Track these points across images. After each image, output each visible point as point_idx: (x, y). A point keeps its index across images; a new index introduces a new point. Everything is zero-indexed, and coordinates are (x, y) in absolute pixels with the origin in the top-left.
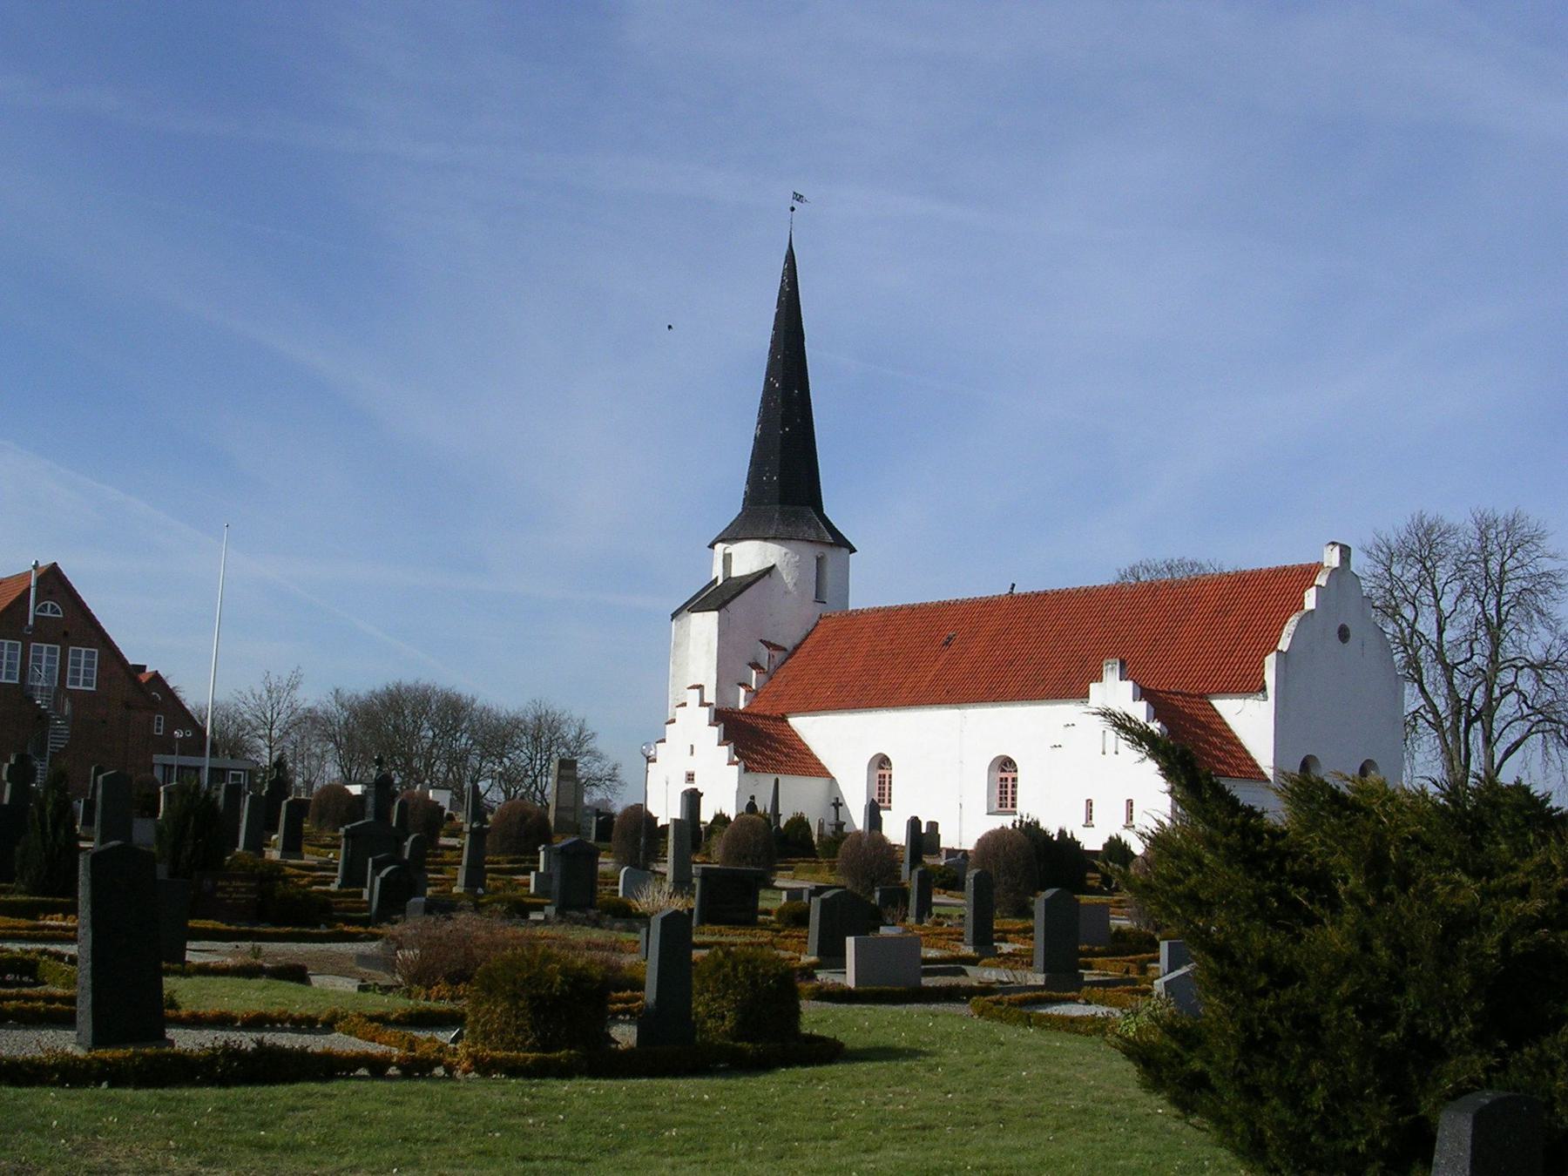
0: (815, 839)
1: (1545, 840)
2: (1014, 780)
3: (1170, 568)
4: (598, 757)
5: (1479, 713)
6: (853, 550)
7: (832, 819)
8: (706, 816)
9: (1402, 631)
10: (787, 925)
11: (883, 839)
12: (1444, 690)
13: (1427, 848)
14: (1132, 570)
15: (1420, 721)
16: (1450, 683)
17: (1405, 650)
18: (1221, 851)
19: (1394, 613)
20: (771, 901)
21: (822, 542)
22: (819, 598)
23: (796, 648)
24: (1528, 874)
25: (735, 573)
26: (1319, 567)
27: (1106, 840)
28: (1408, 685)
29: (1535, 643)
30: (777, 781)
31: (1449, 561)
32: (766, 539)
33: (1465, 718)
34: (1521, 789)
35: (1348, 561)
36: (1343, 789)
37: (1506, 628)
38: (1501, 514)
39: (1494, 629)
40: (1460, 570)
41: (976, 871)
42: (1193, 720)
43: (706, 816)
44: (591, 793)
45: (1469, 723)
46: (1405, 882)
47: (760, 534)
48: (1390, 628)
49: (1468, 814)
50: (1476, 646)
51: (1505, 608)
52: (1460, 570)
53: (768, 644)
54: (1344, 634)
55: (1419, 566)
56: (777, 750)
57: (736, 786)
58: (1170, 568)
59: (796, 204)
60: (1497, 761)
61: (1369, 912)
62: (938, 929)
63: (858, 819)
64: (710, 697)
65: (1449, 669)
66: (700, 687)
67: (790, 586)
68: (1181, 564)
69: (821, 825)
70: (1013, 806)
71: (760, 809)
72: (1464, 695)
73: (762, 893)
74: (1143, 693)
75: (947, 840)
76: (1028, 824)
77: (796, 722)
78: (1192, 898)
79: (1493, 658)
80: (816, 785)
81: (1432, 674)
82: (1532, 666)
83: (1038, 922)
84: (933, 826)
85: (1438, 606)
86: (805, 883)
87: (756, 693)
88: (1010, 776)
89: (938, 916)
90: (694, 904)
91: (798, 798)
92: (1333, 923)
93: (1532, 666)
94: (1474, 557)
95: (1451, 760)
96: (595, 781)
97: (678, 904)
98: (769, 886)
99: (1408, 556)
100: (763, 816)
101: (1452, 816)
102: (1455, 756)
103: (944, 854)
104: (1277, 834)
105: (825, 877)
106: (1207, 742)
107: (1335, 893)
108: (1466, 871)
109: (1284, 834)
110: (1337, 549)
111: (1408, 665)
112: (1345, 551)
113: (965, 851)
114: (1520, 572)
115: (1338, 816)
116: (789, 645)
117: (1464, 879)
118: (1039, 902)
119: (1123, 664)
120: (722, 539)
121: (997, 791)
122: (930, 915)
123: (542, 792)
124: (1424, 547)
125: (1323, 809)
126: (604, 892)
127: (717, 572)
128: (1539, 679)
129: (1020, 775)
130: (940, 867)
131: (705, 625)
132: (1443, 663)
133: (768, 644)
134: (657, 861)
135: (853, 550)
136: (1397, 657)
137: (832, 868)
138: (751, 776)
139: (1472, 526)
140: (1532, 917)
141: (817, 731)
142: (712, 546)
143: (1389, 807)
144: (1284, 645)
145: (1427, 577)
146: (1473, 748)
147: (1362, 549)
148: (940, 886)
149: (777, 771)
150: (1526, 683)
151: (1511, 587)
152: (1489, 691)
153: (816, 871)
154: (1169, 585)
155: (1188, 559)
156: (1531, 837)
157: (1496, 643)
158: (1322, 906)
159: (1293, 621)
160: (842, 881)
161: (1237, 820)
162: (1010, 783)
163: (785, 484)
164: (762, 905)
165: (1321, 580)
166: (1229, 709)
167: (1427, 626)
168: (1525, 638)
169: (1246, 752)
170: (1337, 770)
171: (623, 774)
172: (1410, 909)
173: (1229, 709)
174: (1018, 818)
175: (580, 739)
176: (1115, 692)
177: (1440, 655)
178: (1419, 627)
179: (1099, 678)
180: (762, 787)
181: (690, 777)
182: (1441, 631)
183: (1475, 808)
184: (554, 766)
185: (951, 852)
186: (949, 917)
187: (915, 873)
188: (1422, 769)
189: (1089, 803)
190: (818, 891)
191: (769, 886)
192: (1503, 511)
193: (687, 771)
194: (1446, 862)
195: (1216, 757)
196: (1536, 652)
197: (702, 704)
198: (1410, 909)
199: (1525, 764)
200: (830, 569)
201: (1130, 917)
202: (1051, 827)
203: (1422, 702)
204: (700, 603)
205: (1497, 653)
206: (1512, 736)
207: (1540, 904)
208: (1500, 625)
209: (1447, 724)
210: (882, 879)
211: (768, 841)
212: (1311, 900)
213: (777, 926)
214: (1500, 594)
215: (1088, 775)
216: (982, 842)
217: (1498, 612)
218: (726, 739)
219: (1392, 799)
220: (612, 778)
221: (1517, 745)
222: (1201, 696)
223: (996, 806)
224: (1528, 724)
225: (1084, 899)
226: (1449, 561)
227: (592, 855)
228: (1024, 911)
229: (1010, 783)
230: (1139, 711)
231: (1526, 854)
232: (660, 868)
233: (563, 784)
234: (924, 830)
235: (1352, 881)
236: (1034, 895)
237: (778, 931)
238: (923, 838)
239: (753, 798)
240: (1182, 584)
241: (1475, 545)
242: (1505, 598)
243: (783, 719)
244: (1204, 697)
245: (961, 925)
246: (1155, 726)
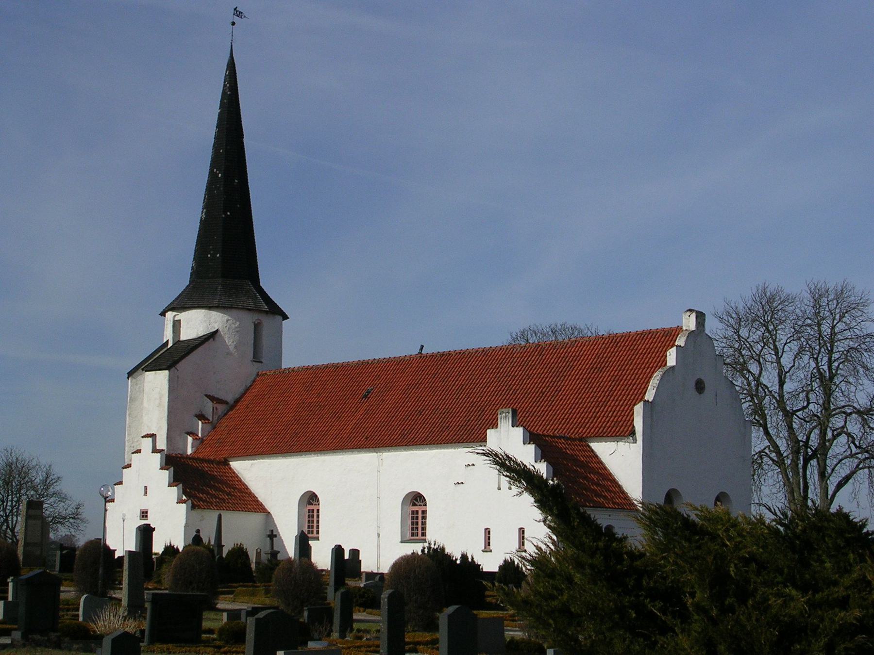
0: (253, 566)
1: (862, 559)
2: (424, 512)
3: (554, 332)
4: (62, 497)
5: (815, 453)
6: (285, 317)
7: (268, 549)
8: (158, 548)
9: (749, 384)
10: (227, 642)
11: (311, 565)
12: (785, 433)
13: (762, 566)
14: (523, 333)
15: (766, 459)
16: (790, 428)
17: (752, 400)
18: (588, 571)
19: (742, 368)
20: (214, 622)
21: (258, 310)
22: (257, 358)
23: (237, 401)
24: (847, 588)
25: (184, 337)
26: (678, 330)
27: (501, 562)
28: (754, 429)
29: (861, 392)
30: (220, 517)
31: (788, 324)
32: (210, 308)
33: (805, 456)
34: (842, 516)
35: (704, 326)
36: (693, 517)
37: (837, 380)
38: (831, 285)
39: (827, 382)
40: (798, 332)
41: (390, 591)
42: (575, 460)
43: (158, 548)
44: (56, 530)
45: (806, 461)
46: (743, 595)
48: (739, 382)
49: (798, 538)
50: (812, 396)
51: (836, 364)
52: (797, 332)
53: (212, 398)
54: (700, 386)
55: (763, 329)
56: (219, 490)
57: (184, 522)
58: (554, 332)
60: (830, 493)
61: (714, 622)
62: (358, 643)
63: (290, 548)
64: (162, 444)
65: (789, 415)
66: (153, 436)
67: (232, 348)
68: (574, 329)
69: (258, 554)
70: (424, 534)
71: (205, 540)
72: (801, 437)
73: (206, 614)
74: (531, 437)
75: (368, 564)
76: (435, 550)
77: (239, 466)
78: (565, 610)
79: (826, 406)
80: (253, 520)
81: (774, 419)
82: (859, 412)
83: (443, 634)
84: (355, 553)
85: (769, 363)
86: (242, 605)
87: (202, 440)
88: (420, 509)
89: (359, 631)
90: (146, 625)
91: (238, 531)
92: (683, 631)
93: (859, 412)
94: (809, 321)
95: (792, 492)
96: (60, 519)
97: (131, 627)
98: (213, 608)
99: (754, 321)
100: (207, 547)
101: (783, 538)
102: (796, 489)
103: (364, 577)
104: (635, 556)
105: (261, 600)
106: (586, 478)
107: (684, 606)
108: (795, 586)
109: (642, 555)
110: (694, 315)
111: (755, 412)
112: (700, 317)
113: (382, 574)
114: (848, 334)
115: (689, 540)
116: (230, 398)
117: (794, 592)
118: (443, 618)
119: (514, 412)
120: (172, 308)
121: (410, 523)
122: (352, 630)
123: (13, 530)
124: (767, 312)
125: (676, 534)
126: (65, 618)
127: (168, 335)
128: (865, 423)
129: (429, 508)
130: (360, 589)
131: (157, 382)
132: (784, 410)
133: (212, 398)
134: (114, 589)
135: (285, 317)
136: (745, 406)
137: (267, 592)
138: (197, 513)
139: (807, 295)
140: (852, 624)
141: (256, 473)
142: (163, 314)
143: (732, 532)
144: (650, 396)
145: (769, 338)
146: (810, 482)
147: (715, 315)
148: (361, 605)
149: (220, 508)
150: (854, 427)
151: (841, 346)
152: (823, 434)
153: (253, 594)
154: (553, 346)
155: (570, 323)
156: (851, 556)
157: (828, 394)
158: (674, 617)
159: (657, 376)
160: (276, 602)
161: (601, 544)
162: (420, 515)
163: (226, 262)
164: (206, 624)
165: (681, 341)
166: (603, 449)
167: (770, 379)
168: (853, 388)
169: (620, 487)
170: (695, 501)
171: (85, 513)
172: (749, 619)
173: (603, 449)
174: (426, 545)
175: (47, 483)
176: (509, 439)
177: (781, 403)
178: (764, 380)
179: (494, 425)
180: (207, 522)
181: (144, 514)
182: (782, 383)
183: (804, 531)
184: (23, 507)
185: (370, 575)
186: (367, 631)
187: (339, 594)
188: (768, 499)
189: (488, 532)
190: (253, 612)
191: (213, 608)
192: (833, 282)
193: (142, 507)
194: (779, 579)
195: (594, 490)
196: (862, 400)
197: (155, 450)
198: (749, 619)
199: (855, 494)
200: (265, 332)
201: (522, 629)
202: (455, 551)
203: (767, 443)
204: (152, 363)
205: (829, 402)
206: (843, 471)
207: (857, 613)
208: (832, 378)
209: (788, 462)
210: (314, 596)
211: (209, 568)
212: (664, 611)
213: (218, 643)
214: (831, 352)
215: (480, 507)
216: (500, 567)
217: (830, 367)
218: (175, 481)
219: (735, 525)
220: (76, 516)
221: (847, 479)
222: (581, 439)
223: (408, 536)
224: (856, 461)
225: (484, 614)
226: (788, 324)
227: (54, 584)
228: (431, 626)
229: (420, 515)
230: (526, 455)
231: (847, 571)
232: (117, 594)
233: (29, 522)
234: (347, 557)
235: (698, 595)
236: (440, 611)
237: (219, 647)
238: (346, 563)
239: (198, 531)
240: (564, 345)
241: (810, 311)
242: (835, 356)
243: (226, 463)
244: (583, 441)
245: (378, 638)
246: (542, 468)
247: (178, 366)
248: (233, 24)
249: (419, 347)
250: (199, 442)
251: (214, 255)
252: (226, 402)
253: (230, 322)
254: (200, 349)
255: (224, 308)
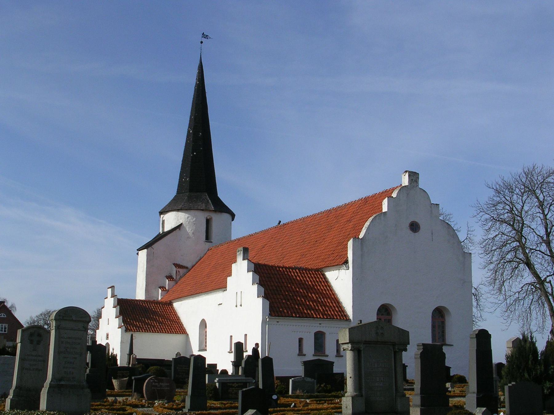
30: (132, 335)
32: (178, 210)
47: (175, 208)
53: (176, 265)
54: (414, 227)
59: (204, 40)
67: (191, 234)
110: (407, 174)
116: (189, 265)
133: (176, 265)
163: (198, 184)
166: (331, 275)
222: (317, 270)
243: (170, 304)
247: (153, 246)
248: (202, 42)
249: (278, 222)
250: (166, 292)
251: (186, 179)
252: (187, 268)
253: (190, 218)
254: (169, 236)
255: (186, 209)
